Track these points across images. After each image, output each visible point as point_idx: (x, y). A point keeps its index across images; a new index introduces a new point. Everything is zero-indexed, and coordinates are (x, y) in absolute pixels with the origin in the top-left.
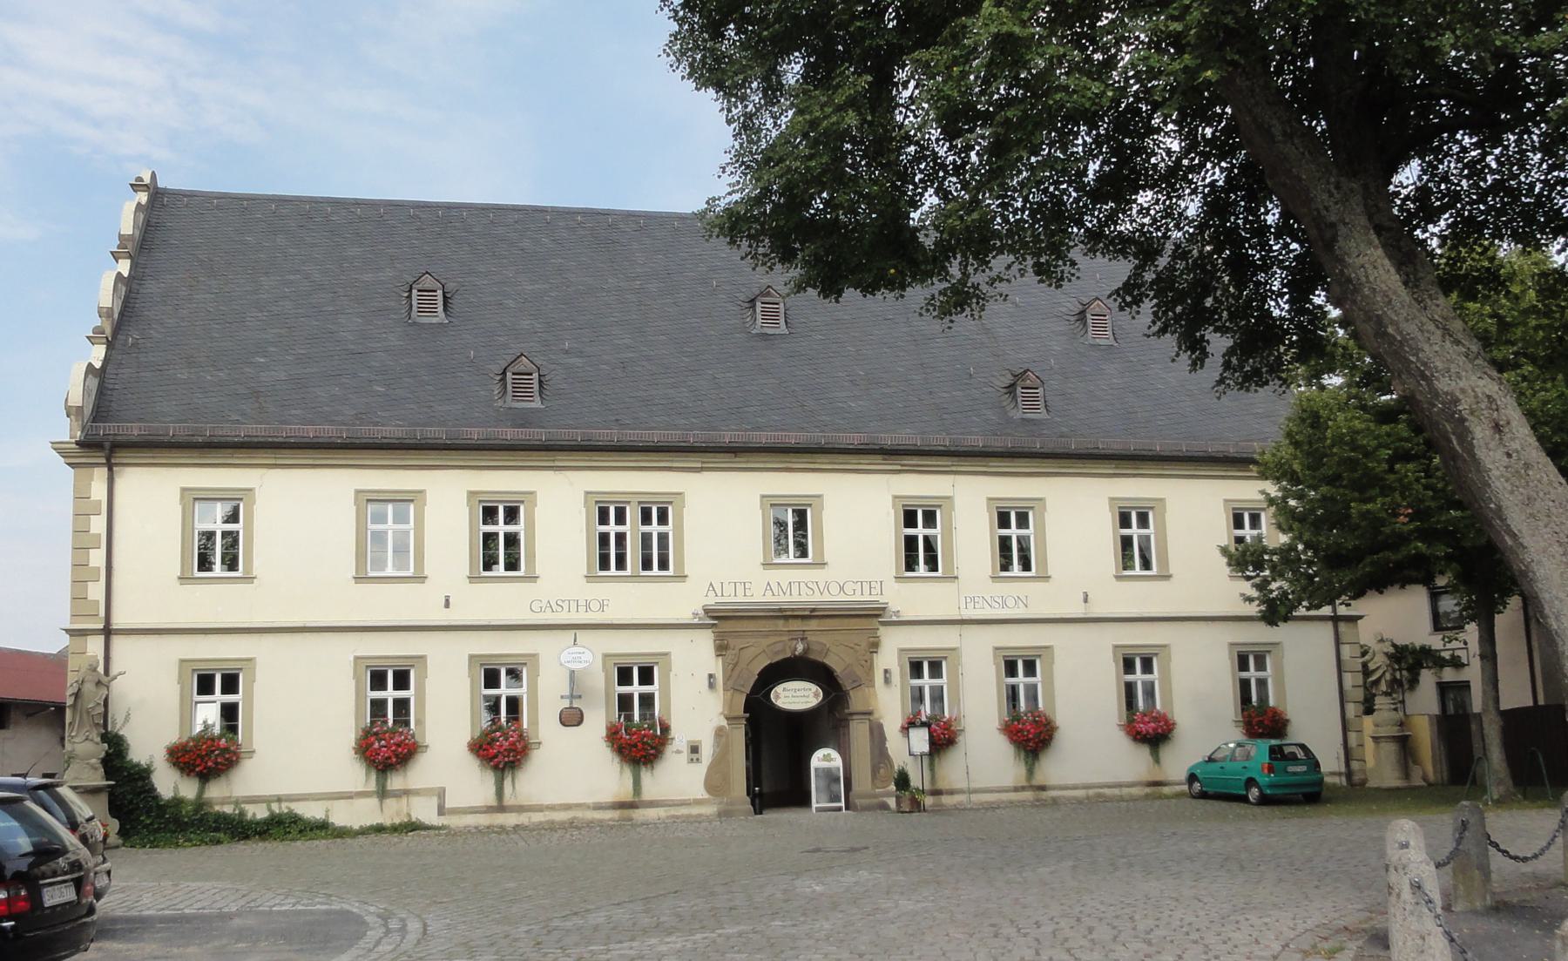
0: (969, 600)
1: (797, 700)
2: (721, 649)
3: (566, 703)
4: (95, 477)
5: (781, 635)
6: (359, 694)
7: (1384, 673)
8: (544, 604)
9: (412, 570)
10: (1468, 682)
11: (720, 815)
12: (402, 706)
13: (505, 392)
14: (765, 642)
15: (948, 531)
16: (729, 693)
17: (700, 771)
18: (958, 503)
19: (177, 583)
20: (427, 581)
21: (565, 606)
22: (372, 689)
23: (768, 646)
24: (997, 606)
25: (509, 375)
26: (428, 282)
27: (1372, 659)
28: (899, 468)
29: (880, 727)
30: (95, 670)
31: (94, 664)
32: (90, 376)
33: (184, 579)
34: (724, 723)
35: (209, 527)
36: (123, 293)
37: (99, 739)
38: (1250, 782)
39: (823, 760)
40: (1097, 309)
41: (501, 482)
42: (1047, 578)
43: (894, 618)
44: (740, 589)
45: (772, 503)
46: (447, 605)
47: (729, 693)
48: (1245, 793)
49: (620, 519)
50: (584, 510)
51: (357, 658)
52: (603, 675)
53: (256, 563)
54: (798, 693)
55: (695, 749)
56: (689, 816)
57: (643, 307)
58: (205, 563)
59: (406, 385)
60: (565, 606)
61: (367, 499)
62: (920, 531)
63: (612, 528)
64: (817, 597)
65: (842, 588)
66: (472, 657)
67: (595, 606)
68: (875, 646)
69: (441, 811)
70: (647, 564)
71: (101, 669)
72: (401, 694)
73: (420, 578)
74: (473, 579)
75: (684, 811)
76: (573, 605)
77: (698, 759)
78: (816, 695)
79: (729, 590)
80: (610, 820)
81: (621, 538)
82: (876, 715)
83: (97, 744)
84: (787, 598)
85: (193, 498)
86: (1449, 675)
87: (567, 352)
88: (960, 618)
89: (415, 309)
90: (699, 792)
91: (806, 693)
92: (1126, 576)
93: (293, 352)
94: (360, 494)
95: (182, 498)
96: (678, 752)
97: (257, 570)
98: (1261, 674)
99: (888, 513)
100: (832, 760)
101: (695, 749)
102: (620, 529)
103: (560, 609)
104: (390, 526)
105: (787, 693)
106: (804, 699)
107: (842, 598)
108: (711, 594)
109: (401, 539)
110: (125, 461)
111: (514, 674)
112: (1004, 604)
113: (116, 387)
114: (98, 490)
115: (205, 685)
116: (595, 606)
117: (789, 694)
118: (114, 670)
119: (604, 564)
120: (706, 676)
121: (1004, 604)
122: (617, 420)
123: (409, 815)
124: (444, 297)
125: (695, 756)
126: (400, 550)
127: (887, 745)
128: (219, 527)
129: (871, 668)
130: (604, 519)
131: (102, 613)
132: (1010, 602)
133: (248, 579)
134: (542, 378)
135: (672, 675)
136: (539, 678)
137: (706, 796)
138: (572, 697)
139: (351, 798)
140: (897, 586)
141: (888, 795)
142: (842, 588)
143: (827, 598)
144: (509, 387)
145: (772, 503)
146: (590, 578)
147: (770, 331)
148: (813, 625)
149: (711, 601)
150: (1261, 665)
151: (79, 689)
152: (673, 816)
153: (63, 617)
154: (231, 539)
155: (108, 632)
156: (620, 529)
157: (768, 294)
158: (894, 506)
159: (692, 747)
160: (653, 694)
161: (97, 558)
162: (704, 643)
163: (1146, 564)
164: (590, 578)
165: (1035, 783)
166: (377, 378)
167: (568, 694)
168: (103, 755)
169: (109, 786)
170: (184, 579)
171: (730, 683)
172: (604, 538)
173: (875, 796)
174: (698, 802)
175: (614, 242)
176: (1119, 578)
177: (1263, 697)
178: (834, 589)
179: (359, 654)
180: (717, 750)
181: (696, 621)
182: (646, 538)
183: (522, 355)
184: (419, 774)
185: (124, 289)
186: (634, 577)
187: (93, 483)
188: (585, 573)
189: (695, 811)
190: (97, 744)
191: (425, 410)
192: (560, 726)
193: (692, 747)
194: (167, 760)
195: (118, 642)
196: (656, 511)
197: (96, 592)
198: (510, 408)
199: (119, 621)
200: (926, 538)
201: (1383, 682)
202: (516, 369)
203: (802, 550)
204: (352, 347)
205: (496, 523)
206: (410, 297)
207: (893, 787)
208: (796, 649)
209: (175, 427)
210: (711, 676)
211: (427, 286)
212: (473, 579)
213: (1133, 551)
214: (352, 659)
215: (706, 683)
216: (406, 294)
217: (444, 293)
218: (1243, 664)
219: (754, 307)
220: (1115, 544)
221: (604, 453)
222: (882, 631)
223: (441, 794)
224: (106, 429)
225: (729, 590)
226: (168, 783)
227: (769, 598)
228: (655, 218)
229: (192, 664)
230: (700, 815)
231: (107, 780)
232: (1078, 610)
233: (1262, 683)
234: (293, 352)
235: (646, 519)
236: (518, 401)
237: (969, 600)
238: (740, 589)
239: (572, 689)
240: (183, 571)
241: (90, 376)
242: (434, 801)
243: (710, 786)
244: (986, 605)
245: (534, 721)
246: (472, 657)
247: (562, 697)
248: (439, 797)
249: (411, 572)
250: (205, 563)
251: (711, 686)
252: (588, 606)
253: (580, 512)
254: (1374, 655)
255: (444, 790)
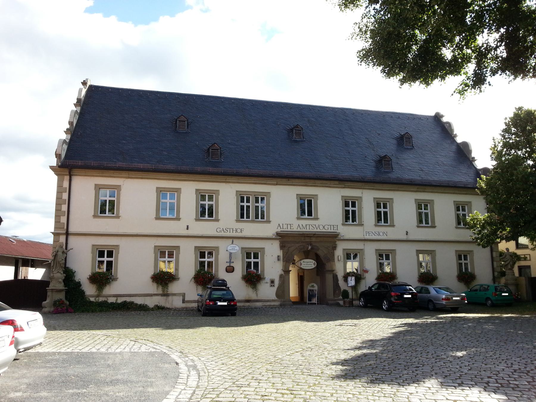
0: (367, 233)
1: (308, 266)
2: (282, 247)
3: (228, 264)
4: (65, 180)
5: (303, 243)
6: (93, 259)
7: (510, 262)
8: (221, 229)
9: (175, 216)
10: (530, 266)
11: (281, 305)
12: (256, 264)
13: (209, 156)
14: (297, 245)
15: (360, 208)
16: (285, 263)
17: (274, 289)
18: (364, 199)
19: (92, 218)
20: (181, 219)
21: (229, 230)
22: (99, 257)
23: (298, 246)
24: (376, 235)
25: (210, 150)
26: (182, 118)
27: (505, 257)
28: (344, 186)
29: (337, 276)
30: (62, 247)
31: (62, 246)
32: (65, 144)
33: (95, 216)
34: (283, 273)
35: (105, 199)
36: (77, 118)
37: (62, 272)
38: (488, 299)
39: (312, 287)
40: (407, 136)
41: (351, 193)
42: (393, 226)
43: (342, 238)
44: (289, 226)
45: (301, 198)
46: (187, 229)
47: (285, 263)
48: (485, 302)
49: (248, 201)
50: (236, 197)
51: (155, 246)
52: (241, 255)
53: (121, 212)
54: (308, 263)
55: (272, 282)
56: (270, 305)
57: (255, 130)
58: (103, 211)
59: (175, 152)
60: (229, 230)
61: (160, 191)
62: (382, 210)
63: (245, 204)
64: (315, 230)
65: (324, 227)
66: (196, 247)
67: (239, 231)
68: (335, 248)
69: (184, 301)
70: (257, 217)
71: (64, 247)
72: (256, 260)
73: (178, 219)
74: (197, 220)
75: (268, 303)
76: (231, 230)
77: (273, 285)
78: (314, 264)
79: (285, 226)
80: (242, 306)
81: (248, 207)
82: (335, 272)
83: (62, 274)
84: (305, 230)
85: (98, 188)
86: (523, 263)
87: (229, 144)
88: (364, 239)
89: (178, 127)
90: (274, 297)
91: (311, 263)
92: (379, 225)
93: (135, 140)
94: (238, 192)
95: (95, 188)
96: (267, 283)
97: (121, 213)
98: (466, 262)
99: (340, 202)
100: (314, 287)
101: (272, 282)
102: (248, 204)
103: (226, 231)
104: (168, 201)
105: (304, 263)
106: (310, 266)
107: (324, 230)
108: (279, 228)
109: (172, 205)
110: (77, 174)
111: (210, 254)
112: (379, 235)
113: (74, 149)
114: (66, 184)
115: (163, 254)
116: (239, 231)
117: (305, 263)
118: (69, 247)
119: (242, 217)
120: (277, 256)
121: (379, 235)
122: (247, 167)
123: (172, 304)
124: (188, 124)
125: (272, 284)
126: (172, 209)
127: (339, 282)
128: (108, 199)
129: (334, 255)
130: (242, 201)
131: (65, 227)
132: (381, 234)
133: (118, 217)
134: (221, 152)
135: (265, 255)
136: (180, 255)
137: (276, 299)
138: (230, 262)
139: (152, 296)
140: (342, 227)
141: (340, 300)
142: (324, 227)
143: (318, 230)
144: (210, 154)
145: (301, 198)
146: (237, 221)
147: (298, 140)
148: (314, 239)
149: (279, 230)
150: (466, 259)
151: (56, 254)
152: (265, 305)
153: (51, 227)
154: (112, 203)
155: (67, 234)
156: (248, 204)
157: (297, 127)
158: (342, 199)
159: (273, 281)
160: (112, 261)
161: (64, 208)
162: (276, 245)
163: (427, 223)
164: (237, 221)
165: (116, 298)
166: (164, 149)
167: (229, 261)
168: (64, 278)
169: (66, 289)
170: (95, 216)
171: (285, 259)
172: (242, 207)
173: (335, 300)
174: (273, 301)
175: (245, 109)
176: (418, 227)
177: (466, 269)
178: (321, 227)
179: (156, 245)
180: (280, 283)
181: (274, 237)
182: (257, 207)
183: (215, 143)
184: (174, 288)
185: (78, 116)
186: (253, 221)
187: (64, 181)
188: (236, 219)
189: (272, 304)
190: (62, 274)
191: (181, 161)
192: (234, 272)
193: (273, 281)
194: (242, 280)
195: (71, 239)
196: (259, 198)
197: (64, 220)
198: (211, 161)
199: (72, 230)
200: (384, 212)
201: (509, 265)
202: (213, 148)
203: (310, 214)
204: (156, 139)
205: (349, 207)
206: (176, 123)
207: (341, 297)
208: (308, 248)
209: (93, 163)
210: (278, 256)
211: (182, 120)
212: (197, 220)
213: (114, 210)
214: (153, 246)
215: (277, 259)
216: (174, 123)
217: (188, 122)
218: (460, 257)
219: (292, 131)
220: (375, 214)
221: (117, 173)
222: (338, 243)
223: (184, 295)
224: (71, 162)
225: (285, 226)
226: (89, 290)
227: (299, 230)
228: (201, 96)
229: (96, 246)
230: (274, 305)
231: (65, 287)
232: (404, 237)
233: (466, 264)
234: (135, 140)
235: (257, 201)
236: (213, 159)
237: (367, 233)
238: (289, 226)
239: (230, 260)
240: (237, 219)
241: (65, 144)
242: (181, 298)
243: (277, 295)
244: (373, 235)
245: (217, 270)
246: (196, 247)
247: (227, 262)
248: (183, 296)
249: (214, 218)
250: (103, 211)
251: (278, 260)
252: (236, 231)
253: (234, 198)
254: (506, 256)
255: (185, 294)
